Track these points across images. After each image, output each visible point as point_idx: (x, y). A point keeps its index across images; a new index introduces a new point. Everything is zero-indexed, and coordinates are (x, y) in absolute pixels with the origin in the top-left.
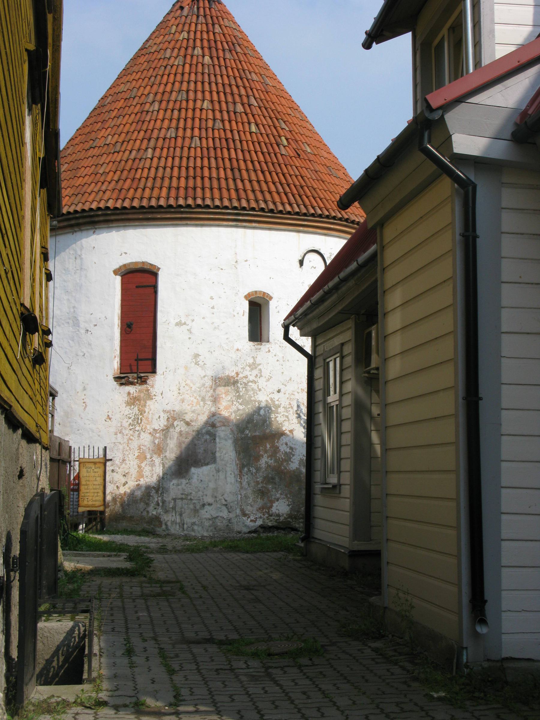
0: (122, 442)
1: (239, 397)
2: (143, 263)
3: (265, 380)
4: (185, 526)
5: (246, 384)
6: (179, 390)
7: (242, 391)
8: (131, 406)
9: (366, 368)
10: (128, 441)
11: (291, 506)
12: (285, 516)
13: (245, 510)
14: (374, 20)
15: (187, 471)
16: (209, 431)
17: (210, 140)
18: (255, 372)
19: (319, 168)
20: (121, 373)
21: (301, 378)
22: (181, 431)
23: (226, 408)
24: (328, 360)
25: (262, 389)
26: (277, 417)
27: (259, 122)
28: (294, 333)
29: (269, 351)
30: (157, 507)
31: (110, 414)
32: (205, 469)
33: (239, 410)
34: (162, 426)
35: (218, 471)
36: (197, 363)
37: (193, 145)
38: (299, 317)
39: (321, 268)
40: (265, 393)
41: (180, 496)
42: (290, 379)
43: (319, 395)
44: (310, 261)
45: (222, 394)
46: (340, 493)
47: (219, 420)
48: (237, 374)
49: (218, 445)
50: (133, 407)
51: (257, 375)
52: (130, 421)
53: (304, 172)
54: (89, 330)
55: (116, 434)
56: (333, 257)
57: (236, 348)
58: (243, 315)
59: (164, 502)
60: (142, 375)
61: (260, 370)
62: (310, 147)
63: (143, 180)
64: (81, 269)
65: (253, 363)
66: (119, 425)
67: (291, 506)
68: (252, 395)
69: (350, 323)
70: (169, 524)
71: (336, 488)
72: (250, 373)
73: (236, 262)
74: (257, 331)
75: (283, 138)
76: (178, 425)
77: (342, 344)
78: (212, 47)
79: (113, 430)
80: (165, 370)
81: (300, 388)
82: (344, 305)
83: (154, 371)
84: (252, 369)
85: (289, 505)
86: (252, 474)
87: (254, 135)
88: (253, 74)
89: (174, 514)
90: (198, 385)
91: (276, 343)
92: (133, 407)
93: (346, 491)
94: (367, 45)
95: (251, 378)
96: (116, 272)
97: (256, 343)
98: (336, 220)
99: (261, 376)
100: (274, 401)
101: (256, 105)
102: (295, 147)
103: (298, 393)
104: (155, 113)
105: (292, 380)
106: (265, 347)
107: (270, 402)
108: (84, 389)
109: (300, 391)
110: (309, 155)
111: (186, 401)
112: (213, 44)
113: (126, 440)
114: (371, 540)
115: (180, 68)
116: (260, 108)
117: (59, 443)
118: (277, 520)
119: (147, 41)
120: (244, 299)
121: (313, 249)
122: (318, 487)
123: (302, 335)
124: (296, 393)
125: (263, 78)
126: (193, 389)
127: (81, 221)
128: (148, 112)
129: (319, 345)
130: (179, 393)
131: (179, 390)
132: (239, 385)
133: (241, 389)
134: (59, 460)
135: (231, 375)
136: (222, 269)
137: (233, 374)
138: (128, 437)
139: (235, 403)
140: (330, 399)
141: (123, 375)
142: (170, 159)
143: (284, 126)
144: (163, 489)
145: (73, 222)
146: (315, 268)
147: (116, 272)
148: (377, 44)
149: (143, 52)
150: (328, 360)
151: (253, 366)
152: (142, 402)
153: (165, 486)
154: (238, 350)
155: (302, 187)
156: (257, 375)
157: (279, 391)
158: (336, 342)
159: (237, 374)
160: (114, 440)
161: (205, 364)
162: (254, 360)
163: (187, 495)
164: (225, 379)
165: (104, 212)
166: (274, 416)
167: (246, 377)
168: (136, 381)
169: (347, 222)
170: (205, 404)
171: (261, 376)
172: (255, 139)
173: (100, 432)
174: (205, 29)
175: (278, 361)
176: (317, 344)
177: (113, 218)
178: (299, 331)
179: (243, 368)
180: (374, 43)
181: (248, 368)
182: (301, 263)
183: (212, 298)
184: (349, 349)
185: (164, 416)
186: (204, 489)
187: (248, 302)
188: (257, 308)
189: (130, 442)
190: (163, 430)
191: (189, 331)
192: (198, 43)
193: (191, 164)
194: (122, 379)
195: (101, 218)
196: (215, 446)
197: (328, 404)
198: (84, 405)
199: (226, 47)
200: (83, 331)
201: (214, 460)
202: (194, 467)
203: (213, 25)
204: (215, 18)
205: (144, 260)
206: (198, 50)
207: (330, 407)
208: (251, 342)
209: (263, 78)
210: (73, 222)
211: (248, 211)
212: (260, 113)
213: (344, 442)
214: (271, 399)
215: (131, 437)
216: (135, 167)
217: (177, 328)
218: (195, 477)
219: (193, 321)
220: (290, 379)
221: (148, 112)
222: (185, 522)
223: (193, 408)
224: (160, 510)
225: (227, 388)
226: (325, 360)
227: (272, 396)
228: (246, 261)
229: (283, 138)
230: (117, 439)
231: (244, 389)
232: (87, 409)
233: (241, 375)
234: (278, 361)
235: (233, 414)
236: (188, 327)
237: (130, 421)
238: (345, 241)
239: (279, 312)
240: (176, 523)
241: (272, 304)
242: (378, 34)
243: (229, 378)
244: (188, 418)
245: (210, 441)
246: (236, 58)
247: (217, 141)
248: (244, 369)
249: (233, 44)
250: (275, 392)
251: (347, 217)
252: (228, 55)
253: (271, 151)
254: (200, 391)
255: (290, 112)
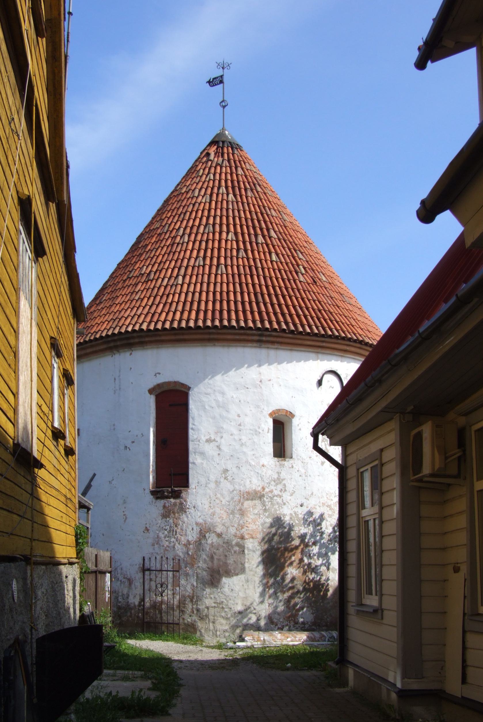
0: (159, 553)
1: (265, 510)
2: (175, 383)
3: (289, 494)
4: (218, 633)
5: (271, 498)
6: (210, 503)
7: (268, 505)
8: (166, 518)
9: (415, 475)
10: (164, 552)
11: (314, 615)
12: (309, 623)
13: (273, 618)
14: (432, 22)
15: (219, 581)
16: (239, 543)
17: (235, 268)
18: (280, 487)
19: (333, 295)
20: (157, 487)
21: (322, 492)
22: (212, 543)
23: (254, 521)
24: (361, 470)
25: (287, 503)
26: (301, 530)
27: (279, 252)
28: (324, 442)
29: (292, 467)
30: (192, 614)
31: (148, 526)
32: (235, 580)
33: (265, 523)
34: (195, 537)
35: (247, 581)
36: (226, 478)
37: (219, 272)
38: (328, 424)
39: (337, 390)
40: (289, 507)
41: (213, 605)
42: (312, 494)
43: (352, 509)
44: (328, 381)
45: (249, 508)
46: (382, 618)
47: (247, 532)
48: (263, 489)
49: (247, 556)
50: (168, 519)
51: (281, 489)
52: (166, 532)
53: (321, 298)
54: (128, 446)
55: (153, 545)
56: (349, 378)
57: (261, 464)
58: (268, 432)
59: (198, 610)
60: (176, 489)
61: (285, 485)
62: (325, 276)
63: (174, 304)
64: (120, 389)
65: (278, 478)
66: (156, 536)
67: (314, 615)
68: (278, 509)
69: (394, 425)
70: (203, 631)
71: (377, 612)
72: (275, 488)
73: (261, 381)
74: (281, 449)
75: (301, 267)
76: (209, 537)
77: (382, 450)
78: (234, 187)
79: (150, 541)
80: (197, 484)
81: (321, 502)
82: (389, 401)
83: (186, 485)
84: (277, 484)
85: (313, 614)
86: (279, 584)
87: (275, 263)
88: (272, 211)
89: (207, 622)
90: (227, 499)
91: (298, 459)
92: (168, 519)
93: (392, 617)
94: (421, 65)
95: (276, 492)
96: (151, 391)
97: (280, 459)
98: (351, 341)
99: (285, 490)
100: (298, 515)
101: (276, 237)
102: (312, 275)
103: (320, 507)
104: (185, 244)
105: (314, 494)
106: (287, 463)
107: (294, 515)
108: (125, 502)
109: (321, 505)
110: (325, 283)
111: (216, 514)
112: (236, 184)
113: (162, 551)
114: (423, 678)
115: (207, 205)
116: (279, 240)
117: (96, 555)
118: (303, 627)
119: (178, 185)
120: (268, 416)
121: (331, 369)
122: (351, 609)
123: (331, 444)
124: (317, 507)
125: (281, 214)
126: (223, 503)
127: (118, 343)
128: (178, 244)
129: (351, 453)
130: (210, 507)
131: (210, 503)
132: (265, 499)
133: (267, 503)
134: (95, 572)
135: (257, 490)
136: (247, 388)
137: (259, 489)
138: (164, 548)
139: (261, 516)
140: (364, 513)
141: (159, 490)
142: (199, 285)
143: (301, 256)
144: (197, 597)
145: (112, 344)
146: (333, 388)
147: (151, 391)
148: (432, 62)
149: (175, 194)
150: (361, 470)
151: (279, 481)
152: (177, 515)
153: (199, 595)
154: (263, 466)
155: (320, 311)
156: (281, 489)
157: (301, 506)
158: (374, 448)
159: (263, 489)
160: (151, 550)
161: (233, 479)
162: (279, 476)
163: (219, 604)
164: (252, 493)
165: (139, 334)
166: (298, 529)
167: (271, 491)
168: (170, 495)
169: (361, 344)
170: (234, 517)
171: (285, 490)
172: (276, 267)
173: (139, 542)
174: (229, 171)
175: (300, 476)
176: (348, 452)
177: (147, 339)
178: (328, 440)
179: (269, 483)
180: (429, 62)
181: (273, 483)
182: (320, 383)
183: (239, 416)
184: (391, 454)
185: (197, 529)
186: (235, 598)
187: (272, 420)
188: (281, 427)
189: (166, 552)
190: (196, 542)
191: (218, 447)
192: (223, 183)
193: (218, 289)
194: (157, 494)
195: (137, 340)
196: (244, 557)
197: (362, 517)
198: (124, 517)
199: (248, 186)
200: (122, 448)
201: (243, 570)
202: (226, 577)
203: (236, 168)
204: (238, 162)
205: (176, 379)
206: (223, 190)
207: (365, 521)
208: (276, 458)
209: (281, 214)
210: (112, 344)
211: (270, 331)
212: (280, 244)
213: (385, 561)
214: (295, 513)
215: (167, 548)
216: (167, 292)
217: (206, 444)
218: (227, 586)
219: (222, 437)
220: (312, 494)
221: (178, 244)
222: (218, 629)
223: (223, 521)
224: (195, 618)
225: (254, 501)
226: (358, 470)
227: (296, 510)
228: (270, 380)
229: (301, 267)
230: (154, 549)
231: (270, 503)
232: (127, 521)
233: (267, 490)
234: (300, 476)
235: (260, 527)
236: (217, 444)
237: (166, 532)
238: (361, 363)
239: (300, 429)
240: (210, 630)
241: (295, 421)
242: (433, 50)
243: (256, 492)
244: (219, 530)
245: (239, 553)
246: (257, 196)
247: (241, 268)
248: (270, 483)
249: (254, 185)
250: (299, 506)
251: (361, 339)
252: (249, 194)
253: (291, 278)
254: (229, 505)
255: (306, 245)
